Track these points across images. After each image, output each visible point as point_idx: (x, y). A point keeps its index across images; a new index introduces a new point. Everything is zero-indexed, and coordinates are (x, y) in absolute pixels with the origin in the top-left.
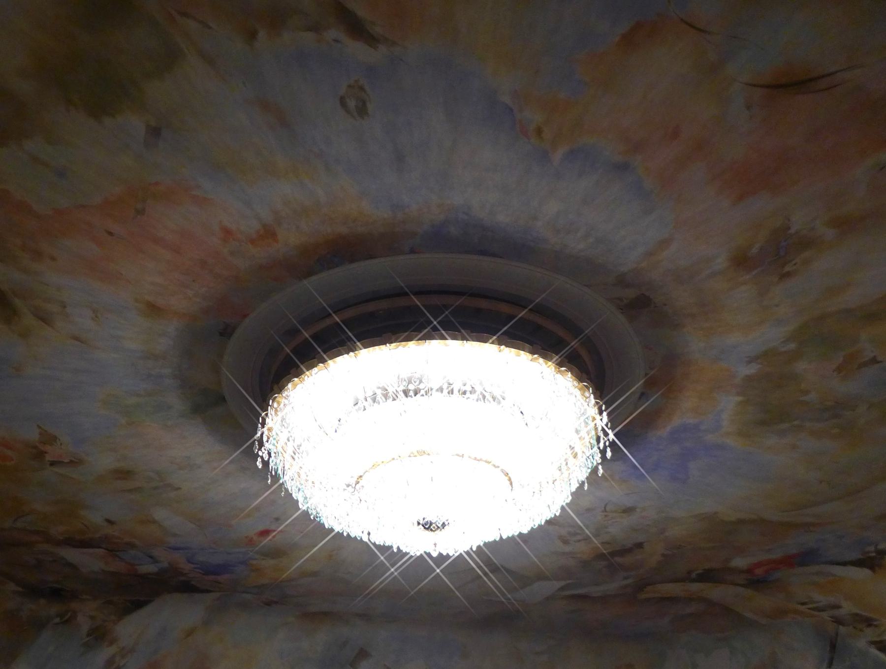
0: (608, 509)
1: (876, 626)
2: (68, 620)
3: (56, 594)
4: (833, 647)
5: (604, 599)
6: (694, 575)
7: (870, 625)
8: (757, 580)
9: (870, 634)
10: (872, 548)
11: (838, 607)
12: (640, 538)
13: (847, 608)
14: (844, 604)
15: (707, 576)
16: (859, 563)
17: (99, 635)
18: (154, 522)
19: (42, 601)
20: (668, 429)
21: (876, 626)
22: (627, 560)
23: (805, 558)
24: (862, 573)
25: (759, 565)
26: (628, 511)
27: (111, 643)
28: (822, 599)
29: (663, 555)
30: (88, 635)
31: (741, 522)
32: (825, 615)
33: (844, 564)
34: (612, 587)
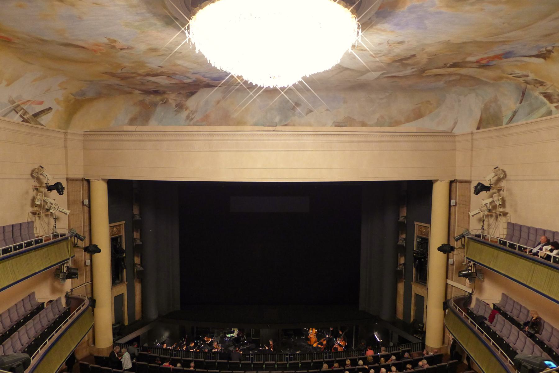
0: (389, 42)
1: (545, 86)
2: (166, 102)
3: (156, 92)
4: (523, 94)
5: (405, 77)
6: (448, 65)
7: (541, 85)
8: (483, 65)
9: (541, 89)
10: (544, 49)
11: (528, 76)
12: (413, 53)
13: (532, 77)
14: (530, 74)
15: (454, 65)
16: (537, 56)
17: (180, 107)
18: (179, 65)
19: (152, 96)
20: (406, 7)
21: (545, 86)
22: (409, 62)
23: (507, 55)
24: (541, 60)
25: (482, 59)
26: (401, 43)
27: (187, 109)
28: (519, 72)
29: (428, 59)
30: (176, 107)
31: (465, 43)
32: (521, 80)
33: (530, 56)
34: (408, 71)
